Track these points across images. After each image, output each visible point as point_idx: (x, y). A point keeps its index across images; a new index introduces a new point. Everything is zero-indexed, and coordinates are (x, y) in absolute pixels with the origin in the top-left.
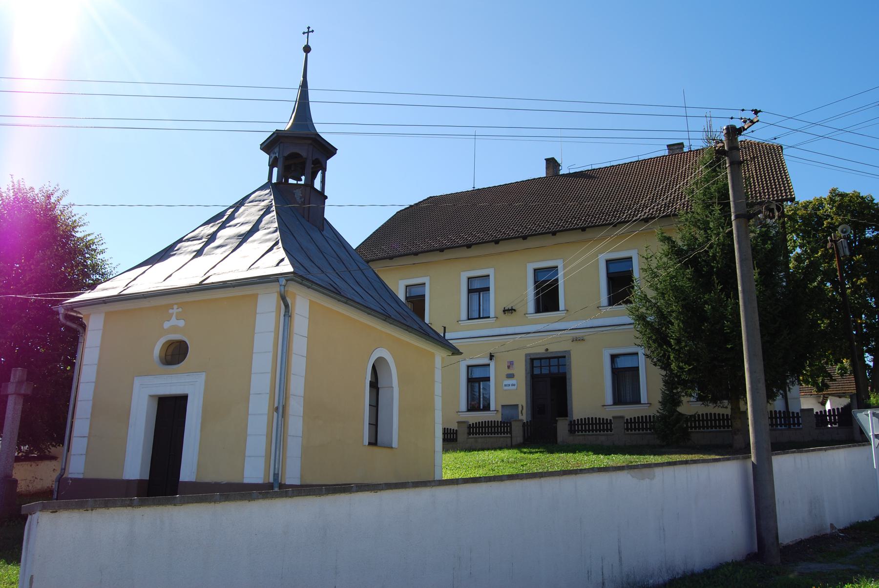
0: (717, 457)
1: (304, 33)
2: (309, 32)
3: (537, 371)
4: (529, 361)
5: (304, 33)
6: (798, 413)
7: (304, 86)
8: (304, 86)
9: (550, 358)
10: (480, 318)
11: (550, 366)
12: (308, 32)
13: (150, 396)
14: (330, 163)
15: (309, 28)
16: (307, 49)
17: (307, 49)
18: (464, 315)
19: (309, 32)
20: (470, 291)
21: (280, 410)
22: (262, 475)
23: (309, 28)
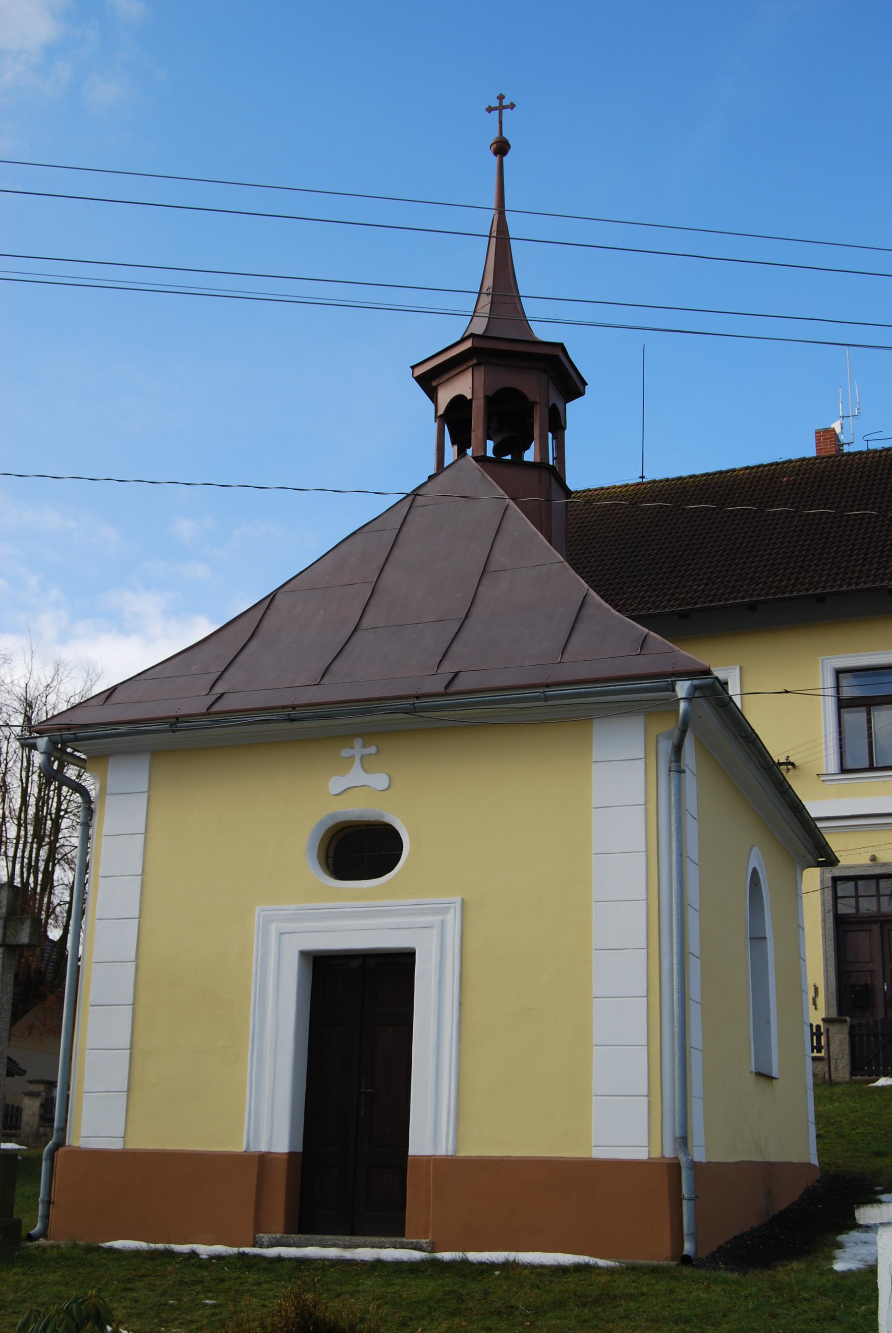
0: (677, 1111)
1: (490, 110)
2: (501, 107)
3: (846, 908)
4: (829, 883)
5: (490, 110)
6: (818, 1027)
7: (501, 238)
8: (501, 238)
9: (877, 877)
10: (871, 768)
11: (857, 897)
12: (501, 108)
13: (16, 1016)
14: (574, 410)
15: (501, 98)
16: (501, 148)
17: (501, 148)
18: (833, 765)
19: (501, 107)
20: (843, 704)
21: (254, 1031)
22: (642, 1138)
23: (501, 98)
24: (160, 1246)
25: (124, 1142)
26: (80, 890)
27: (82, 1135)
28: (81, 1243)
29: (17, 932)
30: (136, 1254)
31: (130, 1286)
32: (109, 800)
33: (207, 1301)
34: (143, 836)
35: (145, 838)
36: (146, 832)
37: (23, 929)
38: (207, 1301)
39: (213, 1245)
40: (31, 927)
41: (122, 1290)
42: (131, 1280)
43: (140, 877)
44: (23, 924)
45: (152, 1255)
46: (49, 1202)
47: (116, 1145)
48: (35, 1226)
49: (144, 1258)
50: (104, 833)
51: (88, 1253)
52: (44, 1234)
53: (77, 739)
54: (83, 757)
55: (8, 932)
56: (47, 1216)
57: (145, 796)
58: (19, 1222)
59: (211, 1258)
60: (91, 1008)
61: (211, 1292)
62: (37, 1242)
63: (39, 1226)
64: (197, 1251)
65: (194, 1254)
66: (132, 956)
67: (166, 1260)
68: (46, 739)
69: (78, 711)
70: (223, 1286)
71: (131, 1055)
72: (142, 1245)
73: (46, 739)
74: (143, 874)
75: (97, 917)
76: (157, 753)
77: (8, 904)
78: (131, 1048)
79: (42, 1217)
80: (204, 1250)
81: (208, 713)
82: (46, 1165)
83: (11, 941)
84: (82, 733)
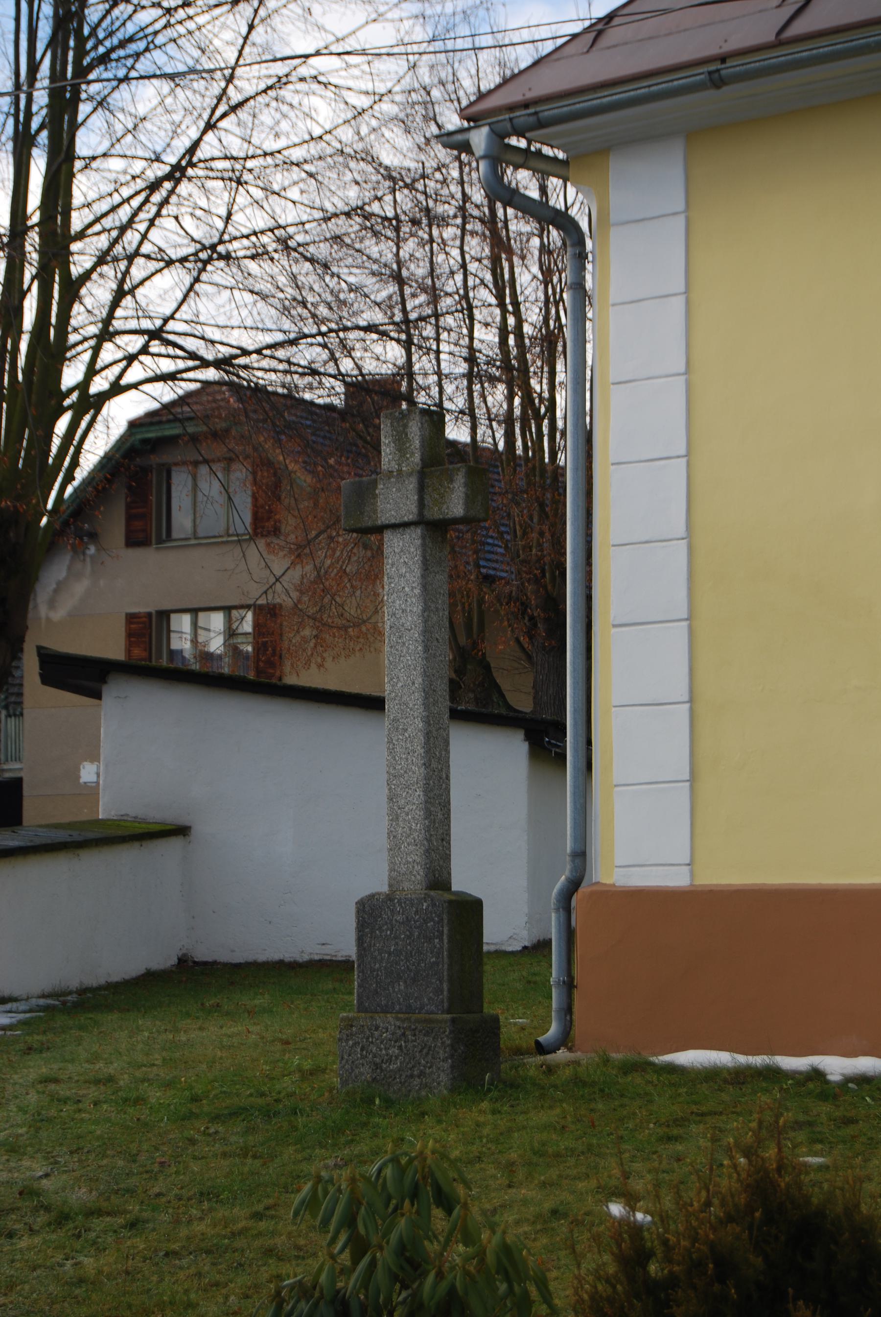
24: (758, 1060)
25: (692, 874)
26: (378, 375)
27: (617, 863)
28: (616, 1056)
29: (442, 496)
30: (712, 1074)
31: (675, 1132)
32: (615, 235)
33: (810, 1159)
34: (682, 298)
35: (688, 302)
36: (687, 291)
37: (452, 490)
38: (810, 1159)
39: (856, 1056)
40: (466, 485)
41: (660, 1139)
42: (680, 1122)
43: (683, 378)
44: (451, 481)
45: (739, 1077)
46: (569, 985)
47: (677, 879)
48: (548, 1030)
49: (725, 1081)
50: (611, 302)
51: (625, 1074)
52: (565, 1040)
53: (541, 124)
54: (561, 155)
55: (427, 499)
56: (568, 1010)
57: (681, 221)
58: (496, 1020)
59: (848, 1079)
60: (614, 630)
61: (821, 1141)
62: (549, 1057)
63: (554, 1029)
64: (821, 1067)
65: (817, 1074)
66: (681, 531)
67: (764, 1085)
68: (485, 130)
69: (543, 71)
70: (850, 1130)
71: (692, 711)
72: (722, 1058)
73: (485, 130)
74: (688, 371)
75: (612, 459)
76: (696, 135)
77: (422, 445)
78: (691, 701)
79: (559, 1011)
80: (836, 1066)
81: (779, 43)
82: (558, 919)
83: (434, 513)
84: (548, 111)
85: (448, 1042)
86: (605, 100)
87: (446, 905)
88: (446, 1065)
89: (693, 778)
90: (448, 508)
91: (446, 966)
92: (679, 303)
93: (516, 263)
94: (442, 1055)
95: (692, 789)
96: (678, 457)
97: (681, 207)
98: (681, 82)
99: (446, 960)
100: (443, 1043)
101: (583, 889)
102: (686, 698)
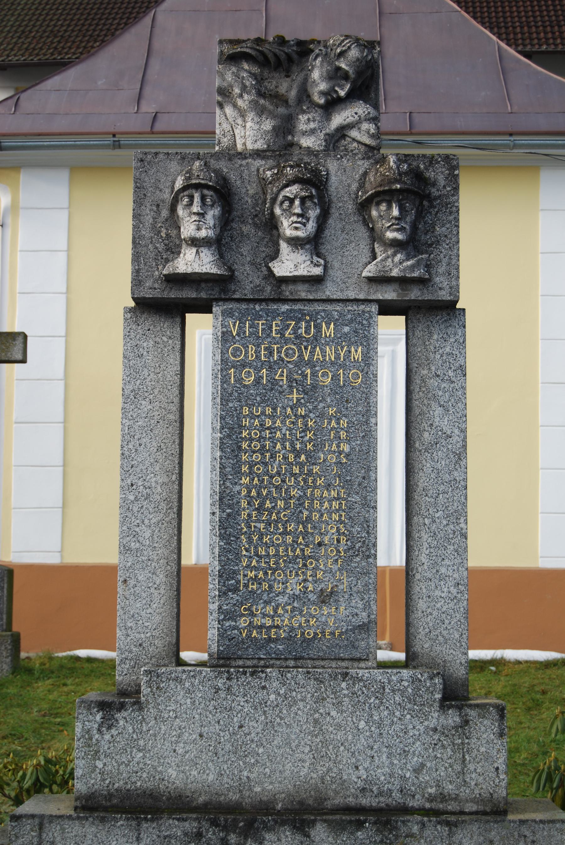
25: (62, 557)
29: (8, 347)
37: (15, 345)
47: (54, 559)
85: (10, 647)
86: (45, 143)
87: (6, 572)
88: (8, 660)
89: (64, 506)
90: (11, 354)
91: (5, 606)
92: (63, 257)
93: (377, 250)
94: (4, 654)
95: (64, 513)
96: (60, 337)
97: (66, 205)
98: (95, 142)
99: (5, 602)
100: (6, 648)
101: (182, 570)
102: (61, 464)
